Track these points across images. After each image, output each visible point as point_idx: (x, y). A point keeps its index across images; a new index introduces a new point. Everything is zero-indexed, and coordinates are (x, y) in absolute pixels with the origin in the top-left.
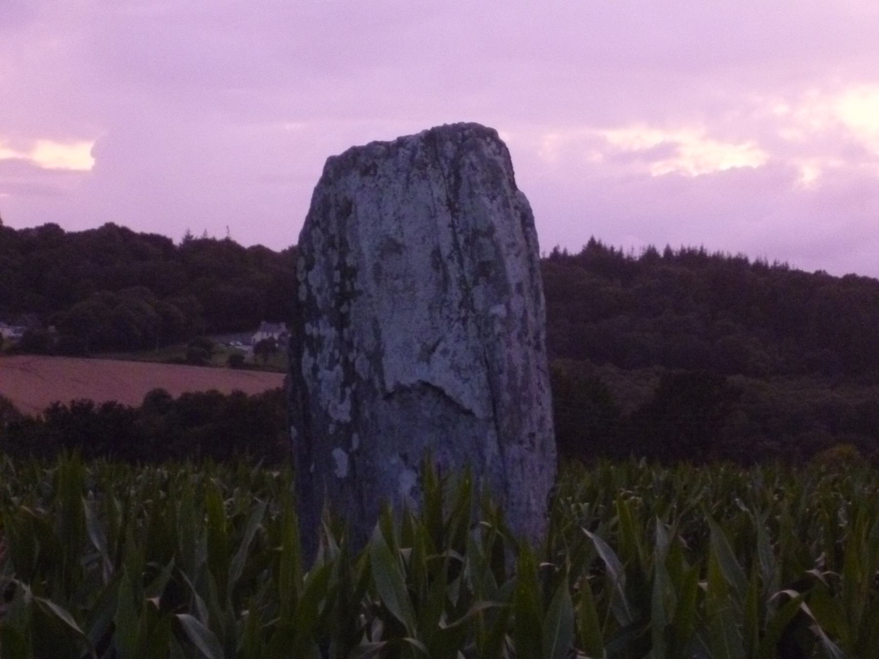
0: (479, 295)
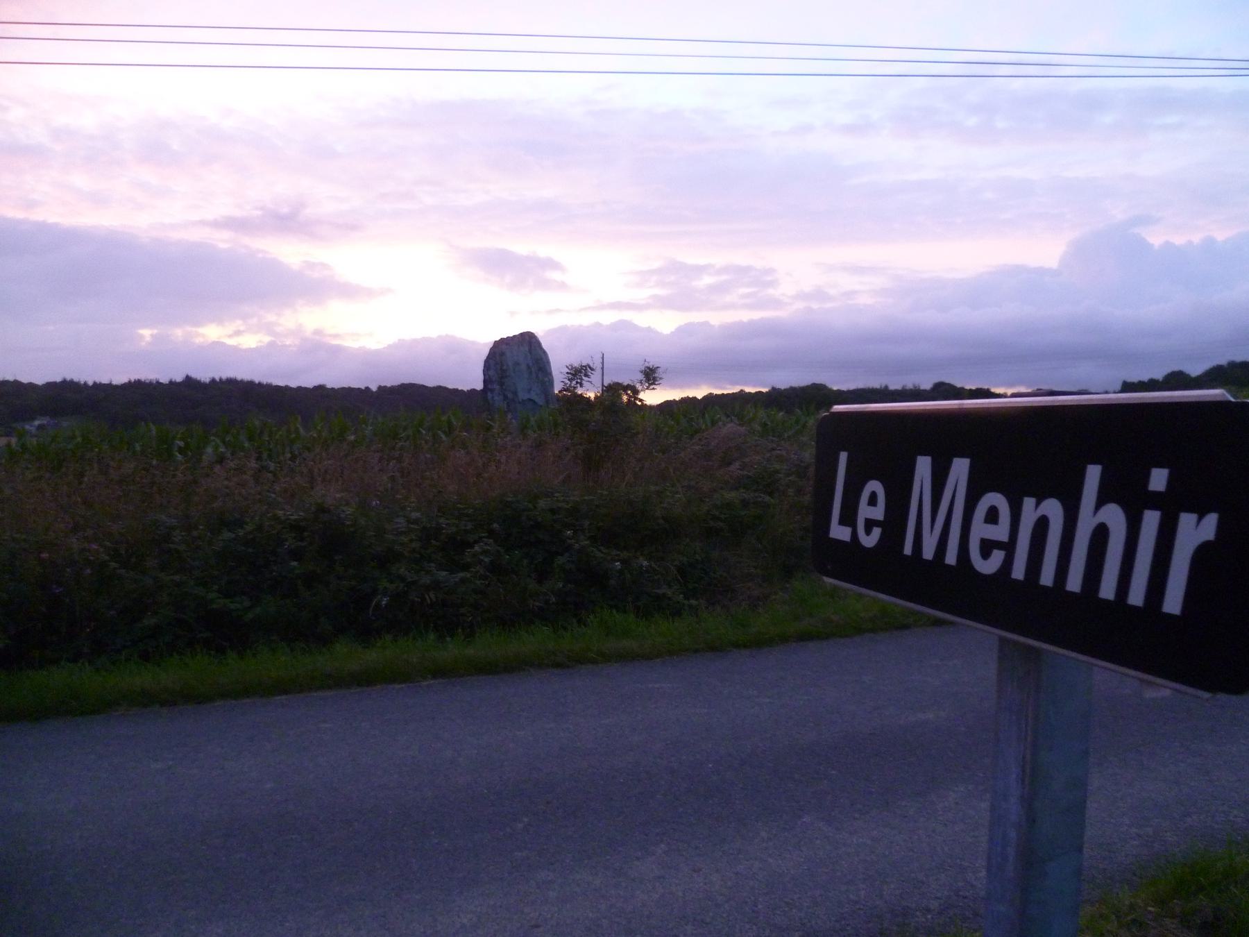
0: (540, 375)
